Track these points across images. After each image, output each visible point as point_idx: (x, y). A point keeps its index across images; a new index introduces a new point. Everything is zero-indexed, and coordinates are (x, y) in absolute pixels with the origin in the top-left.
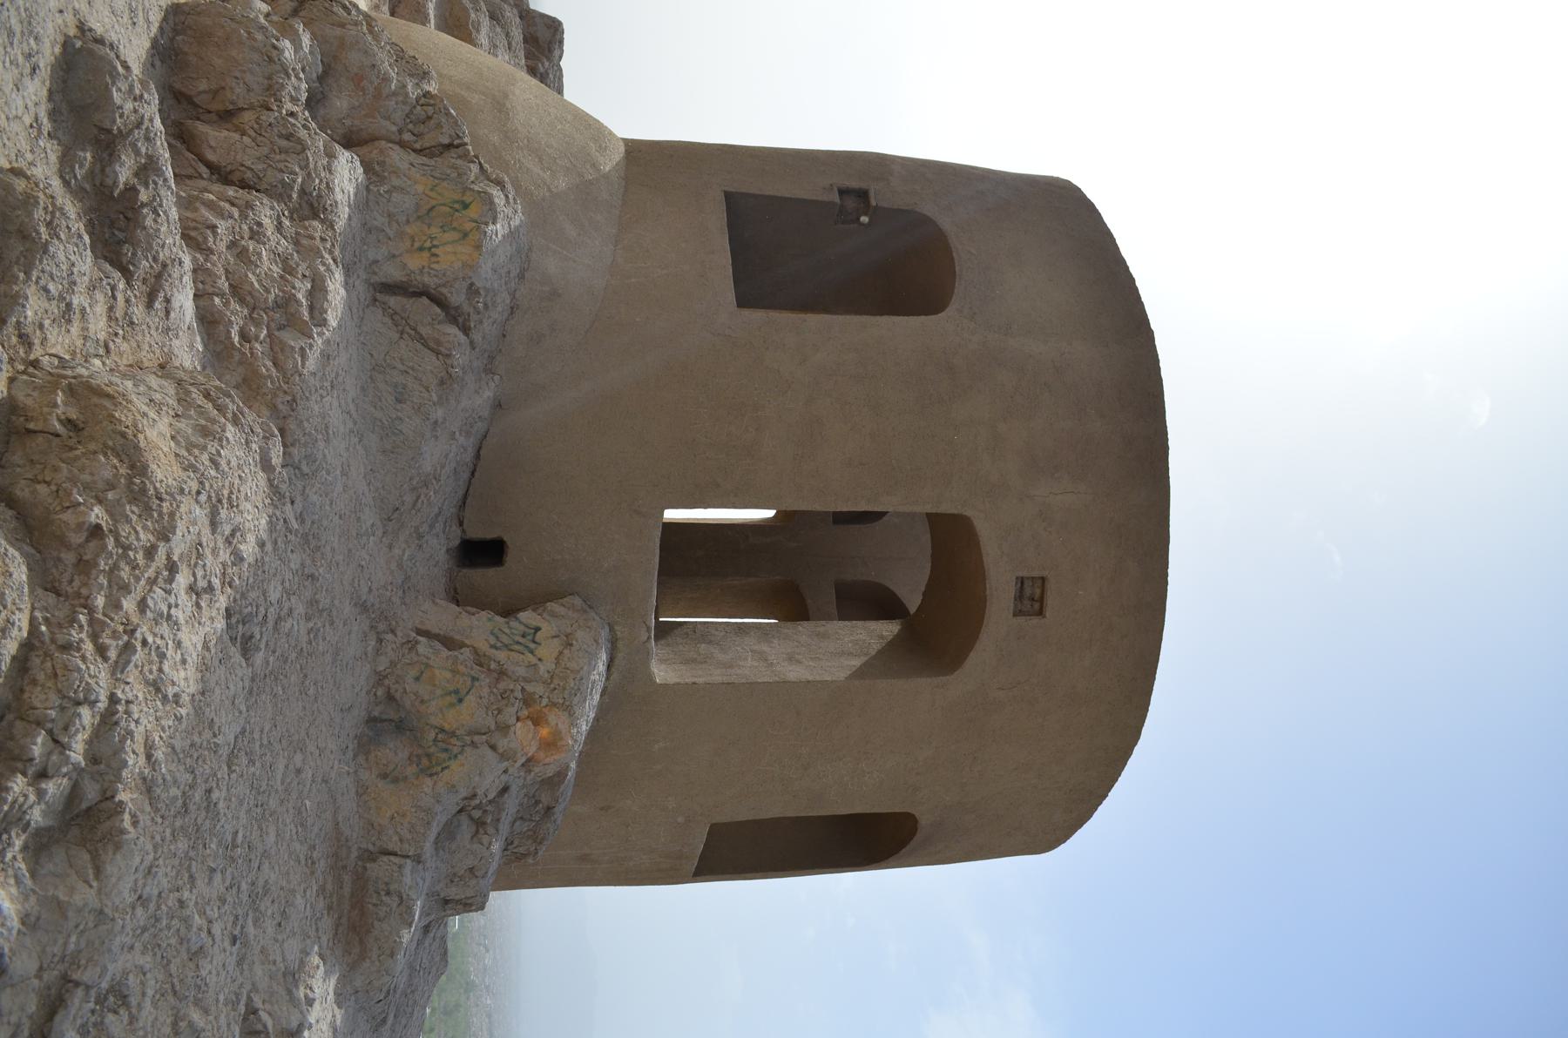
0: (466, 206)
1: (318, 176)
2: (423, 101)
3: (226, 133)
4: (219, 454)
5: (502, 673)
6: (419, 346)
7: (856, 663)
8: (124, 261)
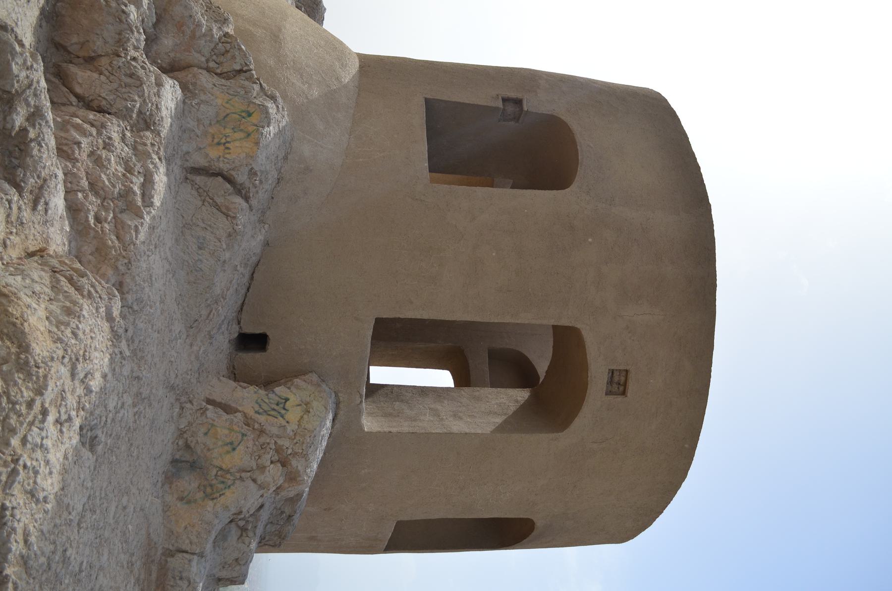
0: (250, 115)
1: (150, 101)
3: (89, 73)
4: (78, 328)
5: (262, 432)
6: (215, 211)
7: (499, 420)
8: (18, 180)
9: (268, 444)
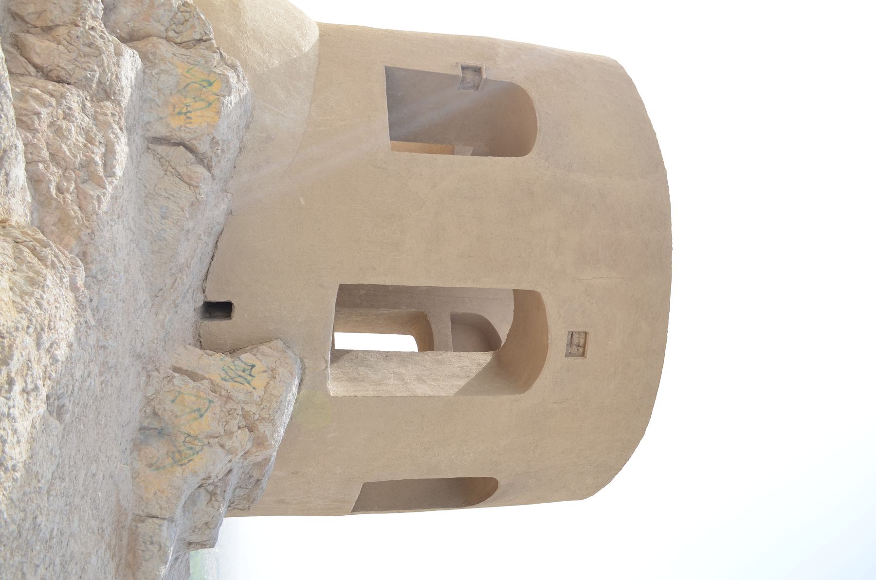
0: (210, 84)
1: (110, 71)
2: (183, 8)
3: (47, 43)
4: (42, 298)
5: (229, 398)
6: (177, 180)
7: (462, 383)
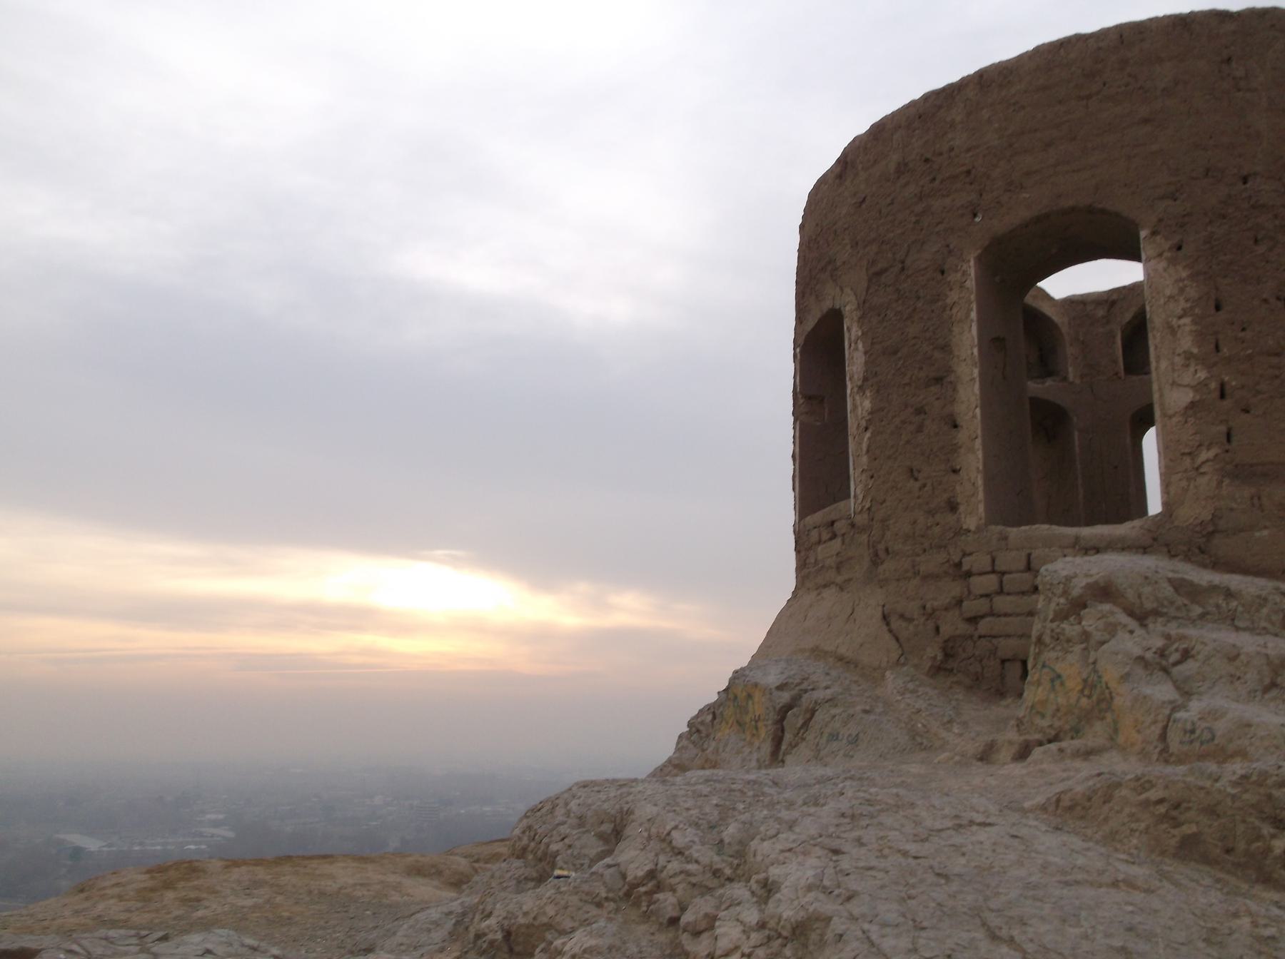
9: (1052, 631)
